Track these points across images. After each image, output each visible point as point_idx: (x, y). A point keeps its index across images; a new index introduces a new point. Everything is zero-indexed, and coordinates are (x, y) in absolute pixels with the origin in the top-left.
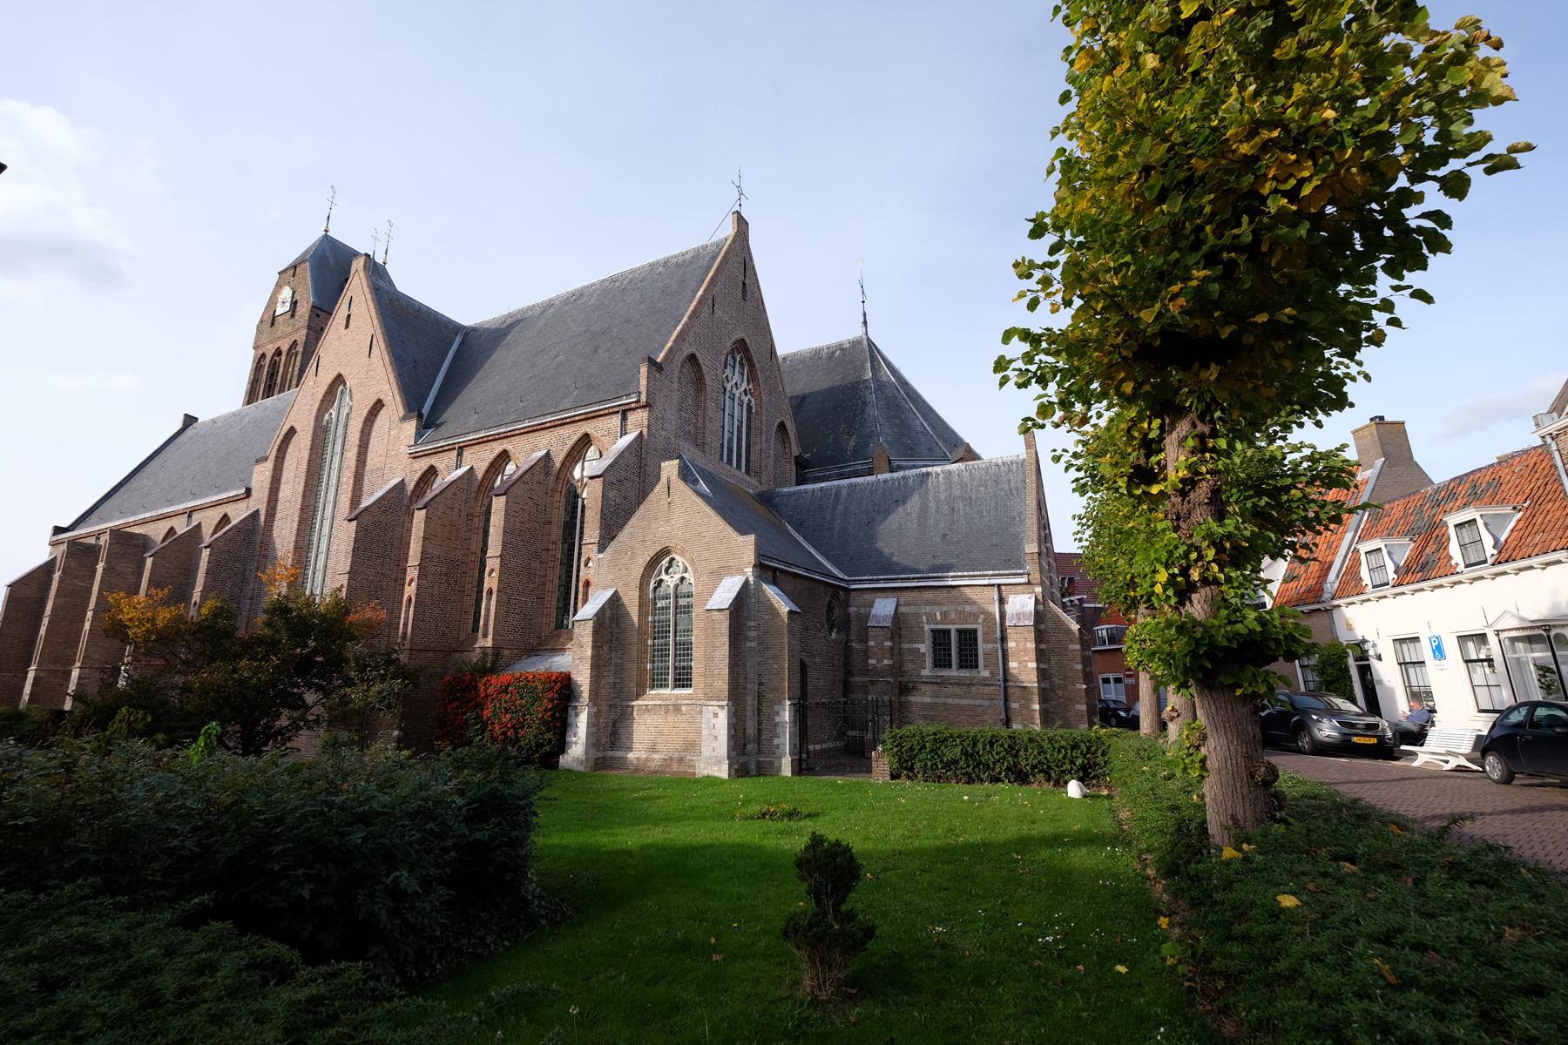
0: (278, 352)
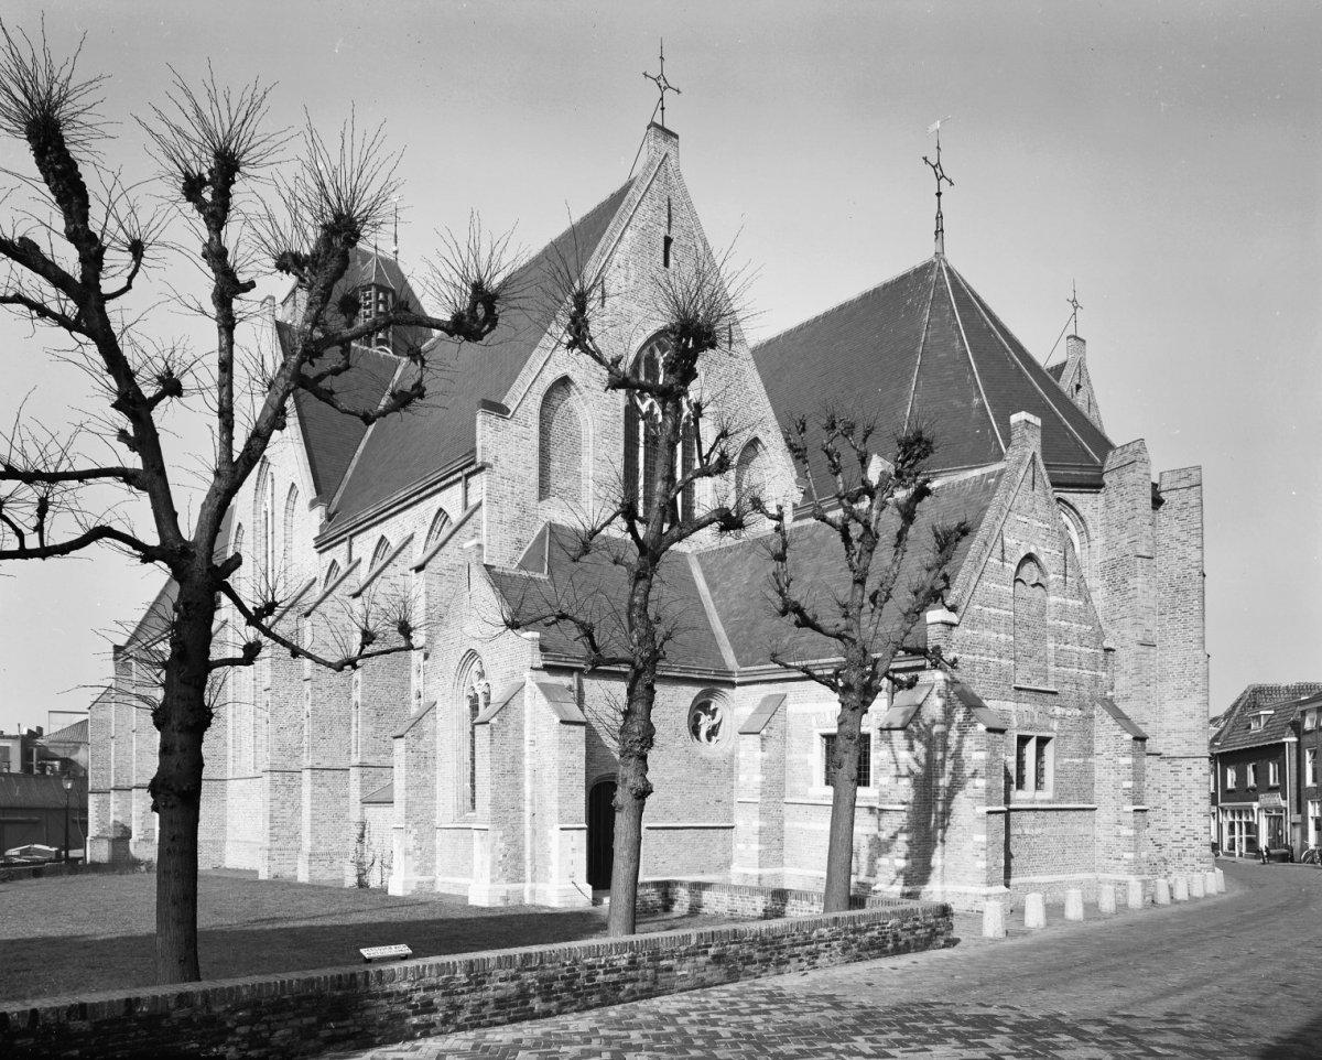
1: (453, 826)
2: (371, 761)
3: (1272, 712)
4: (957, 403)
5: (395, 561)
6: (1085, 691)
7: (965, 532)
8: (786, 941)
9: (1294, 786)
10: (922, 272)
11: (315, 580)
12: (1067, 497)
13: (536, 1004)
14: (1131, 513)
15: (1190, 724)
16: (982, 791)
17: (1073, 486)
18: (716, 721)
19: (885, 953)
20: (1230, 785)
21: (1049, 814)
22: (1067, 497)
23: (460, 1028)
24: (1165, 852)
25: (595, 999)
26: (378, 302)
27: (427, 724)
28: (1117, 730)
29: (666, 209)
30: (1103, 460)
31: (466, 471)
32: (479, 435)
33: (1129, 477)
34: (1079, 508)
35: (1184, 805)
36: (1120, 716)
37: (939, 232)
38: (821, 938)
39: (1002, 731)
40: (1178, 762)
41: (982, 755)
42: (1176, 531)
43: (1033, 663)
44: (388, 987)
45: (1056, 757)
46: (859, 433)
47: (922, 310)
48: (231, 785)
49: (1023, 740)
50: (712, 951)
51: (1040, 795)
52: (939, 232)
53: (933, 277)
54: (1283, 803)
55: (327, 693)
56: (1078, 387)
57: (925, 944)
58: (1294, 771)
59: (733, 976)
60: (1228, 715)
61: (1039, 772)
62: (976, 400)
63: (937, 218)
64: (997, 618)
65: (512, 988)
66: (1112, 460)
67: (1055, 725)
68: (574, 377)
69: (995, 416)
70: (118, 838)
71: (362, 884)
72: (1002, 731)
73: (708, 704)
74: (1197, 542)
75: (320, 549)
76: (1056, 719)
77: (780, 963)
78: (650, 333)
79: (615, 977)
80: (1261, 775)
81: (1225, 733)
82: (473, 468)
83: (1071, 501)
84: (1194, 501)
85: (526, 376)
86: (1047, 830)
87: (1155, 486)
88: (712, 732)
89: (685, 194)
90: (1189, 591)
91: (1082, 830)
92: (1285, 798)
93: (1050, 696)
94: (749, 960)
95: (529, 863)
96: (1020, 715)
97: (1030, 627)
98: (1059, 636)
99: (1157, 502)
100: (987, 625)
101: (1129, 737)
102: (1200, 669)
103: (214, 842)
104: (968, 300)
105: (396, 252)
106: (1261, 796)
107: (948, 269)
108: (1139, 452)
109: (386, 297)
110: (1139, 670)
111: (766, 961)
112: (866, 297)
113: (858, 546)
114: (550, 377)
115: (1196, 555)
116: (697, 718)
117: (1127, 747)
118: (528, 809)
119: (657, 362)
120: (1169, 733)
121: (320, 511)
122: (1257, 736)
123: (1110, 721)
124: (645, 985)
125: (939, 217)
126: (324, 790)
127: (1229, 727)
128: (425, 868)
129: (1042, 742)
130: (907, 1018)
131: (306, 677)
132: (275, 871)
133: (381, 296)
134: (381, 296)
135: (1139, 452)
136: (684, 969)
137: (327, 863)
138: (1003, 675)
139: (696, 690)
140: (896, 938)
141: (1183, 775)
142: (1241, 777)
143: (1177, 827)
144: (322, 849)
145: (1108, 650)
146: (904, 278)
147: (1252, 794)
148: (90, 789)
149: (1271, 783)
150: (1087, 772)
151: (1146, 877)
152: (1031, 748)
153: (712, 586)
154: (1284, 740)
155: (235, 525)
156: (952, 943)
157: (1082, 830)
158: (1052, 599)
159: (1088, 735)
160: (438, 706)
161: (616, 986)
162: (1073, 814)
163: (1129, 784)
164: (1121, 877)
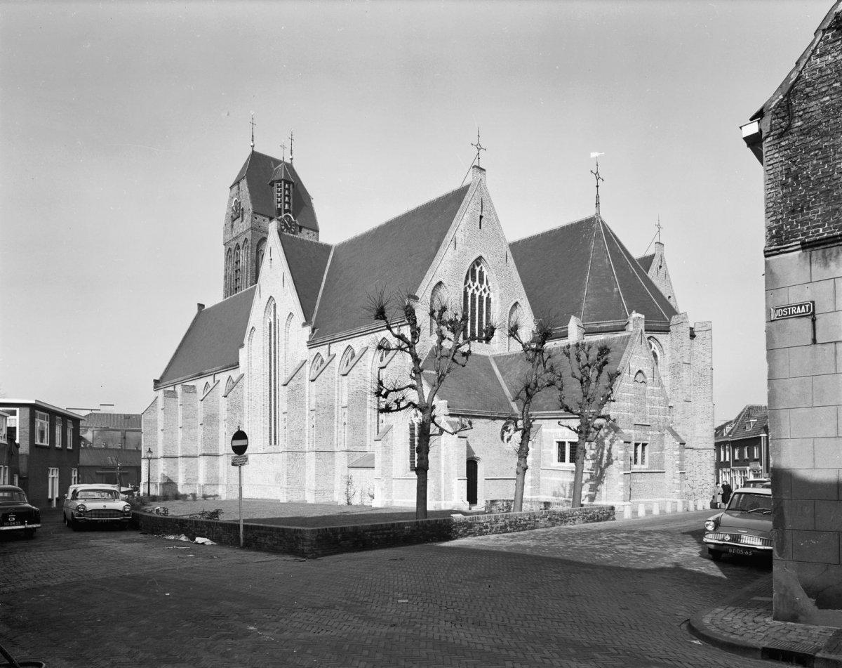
0: (238, 247)
2: (351, 449)
3: (756, 420)
4: (607, 290)
5: (361, 359)
6: (661, 424)
7: (619, 374)
8: (567, 515)
9: (765, 459)
10: (590, 221)
12: (655, 336)
13: (508, 528)
14: (680, 345)
15: (706, 434)
16: (622, 466)
17: (657, 331)
18: (510, 434)
19: (595, 521)
20: (736, 458)
21: (647, 474)
22: (655, 336)
23: (493, 533)
24: (695, 491)
25: (521, 528)
26: (285, 189)
27: (389, 434)
28: (674, 440)
29: (480, 204)
30: (670, 320)
31: (400, 324)
33: (680, 329)
34: (660, 340)
35: (704, 470)
36: (675, 434)
37: (597, 204)
38: (576, 515)
39: (629, 443)
40: (701, 451)
41: (622, 452)
42: (700, 350)
43: (641, 414)
44: (480, 521)
45: (650, 452)
46: (586, 348)
47: (590, 241)
49: (637, 445)
50: (548, 517)
51: (643, 467)
52: (597, 204)
53: (595, 226)
54: (760, 467)
56: (660, 267)
57: (607, 519)
58: (765, 451)
59: (553, 525)
60: (736, 420)
61: (643, 457)
64: (627, 397)
65: (503, 524)
66: (674, 320)
67: (649, 438)
68: (444, 281)
69: (624, 297)
70: (165, 483)
71: (349, 504)
72: (629, 443)
73: (507, 427)
74: (709, 354)
76: (650, 436)
77: (566, 522)
78: (473, 260)
79: (525, 523)
80: (751, 453)
81: (734, 430)
83: (656, 338)
84: (708, 337)
85: (425, 283)
86: (645, 481)
87: (691, 329)
88: (508, 440)
89: (488, 195)
90: (706, 377)
91: (659, 480)
92: (761, 465)
93: (647, 427)
94: (557, 520)
95: (443, 493)
96: (636, 435)
97: (640, 399)
98: (651, 402)
99: (692, 336)
100: (624, 400)
101: (678, 443)
102: (710, 410)
104: (611, 238)
105: (292, 159)
106: (751, 463)
107: (602, 221)
108: (684, 318)
109: (289, 186)
110: (684, 412)
111: (562, 521)
112: (562, 229)
113: (585, 384)
114: (435, 283)
115: (709, 361)
116: (503, 433)
117: (678, 447)
118: (443, 471)
119: (475, 270)
120: (698, 438)
121: (308, 329)
122: (749, 433)
123: (671, 436)
124: (532, 525)
125: (598, 197)
127: (736, 427)
128: (388, 496)
129: (644, 445)
133: (287, 185)
134: (287, 185)
135: (684, 318)
136: (542, 522)
138: (630, 419)
139: (504, 422)
140: (598, 516)
141: (703, 457)
142: (741, 454)
143: (700, 480)
144: (319, 488)
145: (670, 407)
146: (581, 223)
147: (746, 463)
148: (143, 457)
149: (755, 457)
150: (661, 457)
151: (685, 500)
152: (640, 448)
153: (503, 374)
154: (761, 435)
155: (249, 328)
156: (614, 519)
157: (659, 480)
158: (649, 388)
159: (662, 442)
160: (394, 427)
161: (526, 525)
162: (656, 474)
163: (678, 462)
164: (674, 500)
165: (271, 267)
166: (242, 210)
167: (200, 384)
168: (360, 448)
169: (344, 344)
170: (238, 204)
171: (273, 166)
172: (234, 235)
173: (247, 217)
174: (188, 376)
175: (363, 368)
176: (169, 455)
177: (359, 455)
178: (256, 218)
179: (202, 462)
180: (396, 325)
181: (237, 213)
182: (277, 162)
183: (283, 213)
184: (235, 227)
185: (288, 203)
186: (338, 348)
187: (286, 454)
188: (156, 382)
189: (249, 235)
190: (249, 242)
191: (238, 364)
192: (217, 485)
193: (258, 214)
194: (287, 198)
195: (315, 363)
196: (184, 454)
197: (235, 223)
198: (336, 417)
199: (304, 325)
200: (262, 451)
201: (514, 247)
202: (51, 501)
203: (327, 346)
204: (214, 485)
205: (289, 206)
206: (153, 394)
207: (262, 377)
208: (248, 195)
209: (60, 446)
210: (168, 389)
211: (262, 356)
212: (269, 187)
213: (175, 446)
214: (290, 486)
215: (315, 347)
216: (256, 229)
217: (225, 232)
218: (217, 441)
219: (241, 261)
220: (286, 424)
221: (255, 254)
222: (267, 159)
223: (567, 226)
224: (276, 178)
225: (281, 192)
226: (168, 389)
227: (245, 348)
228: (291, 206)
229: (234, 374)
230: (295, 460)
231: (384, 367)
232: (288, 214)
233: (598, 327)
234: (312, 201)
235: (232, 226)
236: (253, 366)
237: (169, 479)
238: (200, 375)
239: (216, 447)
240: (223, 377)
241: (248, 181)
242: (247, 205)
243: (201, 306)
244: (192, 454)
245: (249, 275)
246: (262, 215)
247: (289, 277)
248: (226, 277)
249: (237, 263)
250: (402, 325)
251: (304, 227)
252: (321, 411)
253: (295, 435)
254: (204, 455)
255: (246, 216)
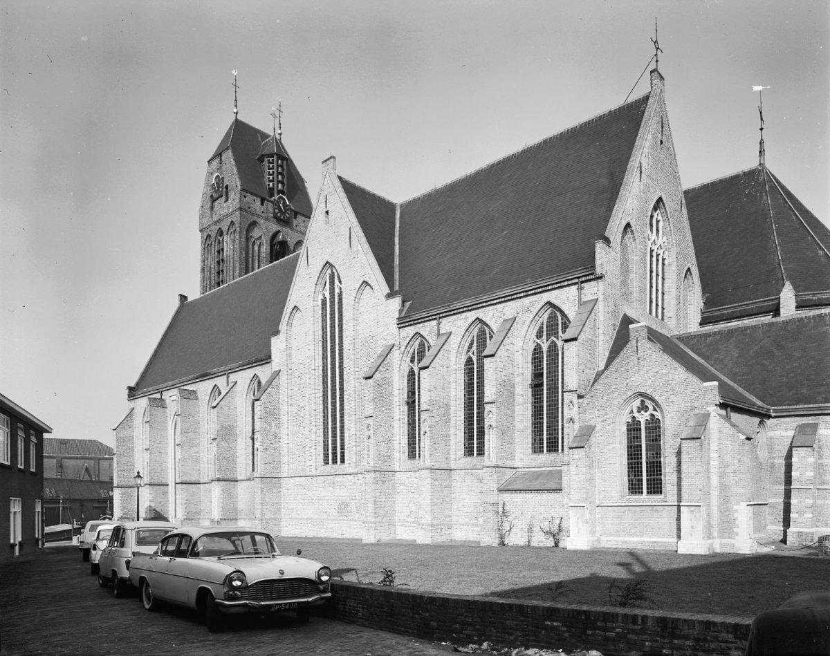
0: (221, 233)
1: (623, 504)
2: (500, 464)
10: (751, 175)
11: (394, 345)
31: (583, 279)
32: (597, 256)
37: (761, 152)
48: (284, 482)
55: (436, 420)
62: (820, 252)
63: (760, 143)
71: (503, 544)
75: (400, 326)
82: (591, 277)
103: (275, 519)
121: (396, 302)
125: (761, 143)
126: (437, 483)
130: (636, 634)
131: (367, 414)
132: (378, 537)
133: (280, 161)
134: (280, 161)
137: (439, 531)
144: (436, 522)
146: (736, 178)
148: (115, 485)
165: (327, 222)
166: (227, 187)
167: (204, 388)
168: (509, 463)
169: (466, 318)
170: (220, 180)
171: (260, 139)
172: (215, 218)
173: (234, 196)
174: (185, 379)
175: (510, 347)
176: (156, 482)
177: (509, 473)
178: (245, 197)
179: (217, 489)
180: (576, 281)
181: (219, 191)
182: (265, 136)
183: (275, 194)
184: (215, 209)
185: (282, 182)
186: (458, 326)
187: (372, 475)
188: (130, 388)
189: (236, 218)
190: (237, 225)
191: (270, 357)
192: (236, 519)
193: (248, 192)
194: (280, 177)
195: (409, 348)
196: (185, 479)
197: (216, 203)
198: (453, 421)
199: (389, 296)
200: (314, 473)
201: (686, 193)
202: (13, 546)
203: (434, 322)
204: (231, 520)
205: (283, 187)
206: (127, 405)
207: (313, 372)
208: (235, 168)
209: (22, 467)
210: (155, 396)
211: (311, 344)
212: (258, 162)
213: (164, 470)
214: (378, 520)
215: (411, 325)
216: (245, 210)
217: (202, 216)
218: (234, 462)
219: (225, 249)
220: (372, 431)
221: (244, 240)
222: (255, 132)
223: (712, 183)
224: (266, 152)
225: (273, 168)
226: (155, 396)
227: (282, 336)
228: (286, 187)
229: (264, 373)
230: (384, 482)
231: (426, 368)
232: (281, 195)
233: (814, 298)
234: (306, 185)
235: (212, 208)
236: (293, 360)
237: (157, 512)
238: (205, 376)
239: (233, 470)
240: (243, 378)
241: (234, 152)
242: (233, 180)
243: (183, 298)
244: (193, 479)
245: (238, 265)
246: (252, 194)
247: (358, 232)
248: (203, 270)
249: (219, 252)
250: (586, 281)
251: (300, 214)
252: (435, 413)
253: (382, 447)
254: (219, 480)
255: (232, 195)
